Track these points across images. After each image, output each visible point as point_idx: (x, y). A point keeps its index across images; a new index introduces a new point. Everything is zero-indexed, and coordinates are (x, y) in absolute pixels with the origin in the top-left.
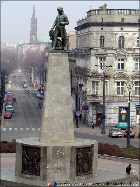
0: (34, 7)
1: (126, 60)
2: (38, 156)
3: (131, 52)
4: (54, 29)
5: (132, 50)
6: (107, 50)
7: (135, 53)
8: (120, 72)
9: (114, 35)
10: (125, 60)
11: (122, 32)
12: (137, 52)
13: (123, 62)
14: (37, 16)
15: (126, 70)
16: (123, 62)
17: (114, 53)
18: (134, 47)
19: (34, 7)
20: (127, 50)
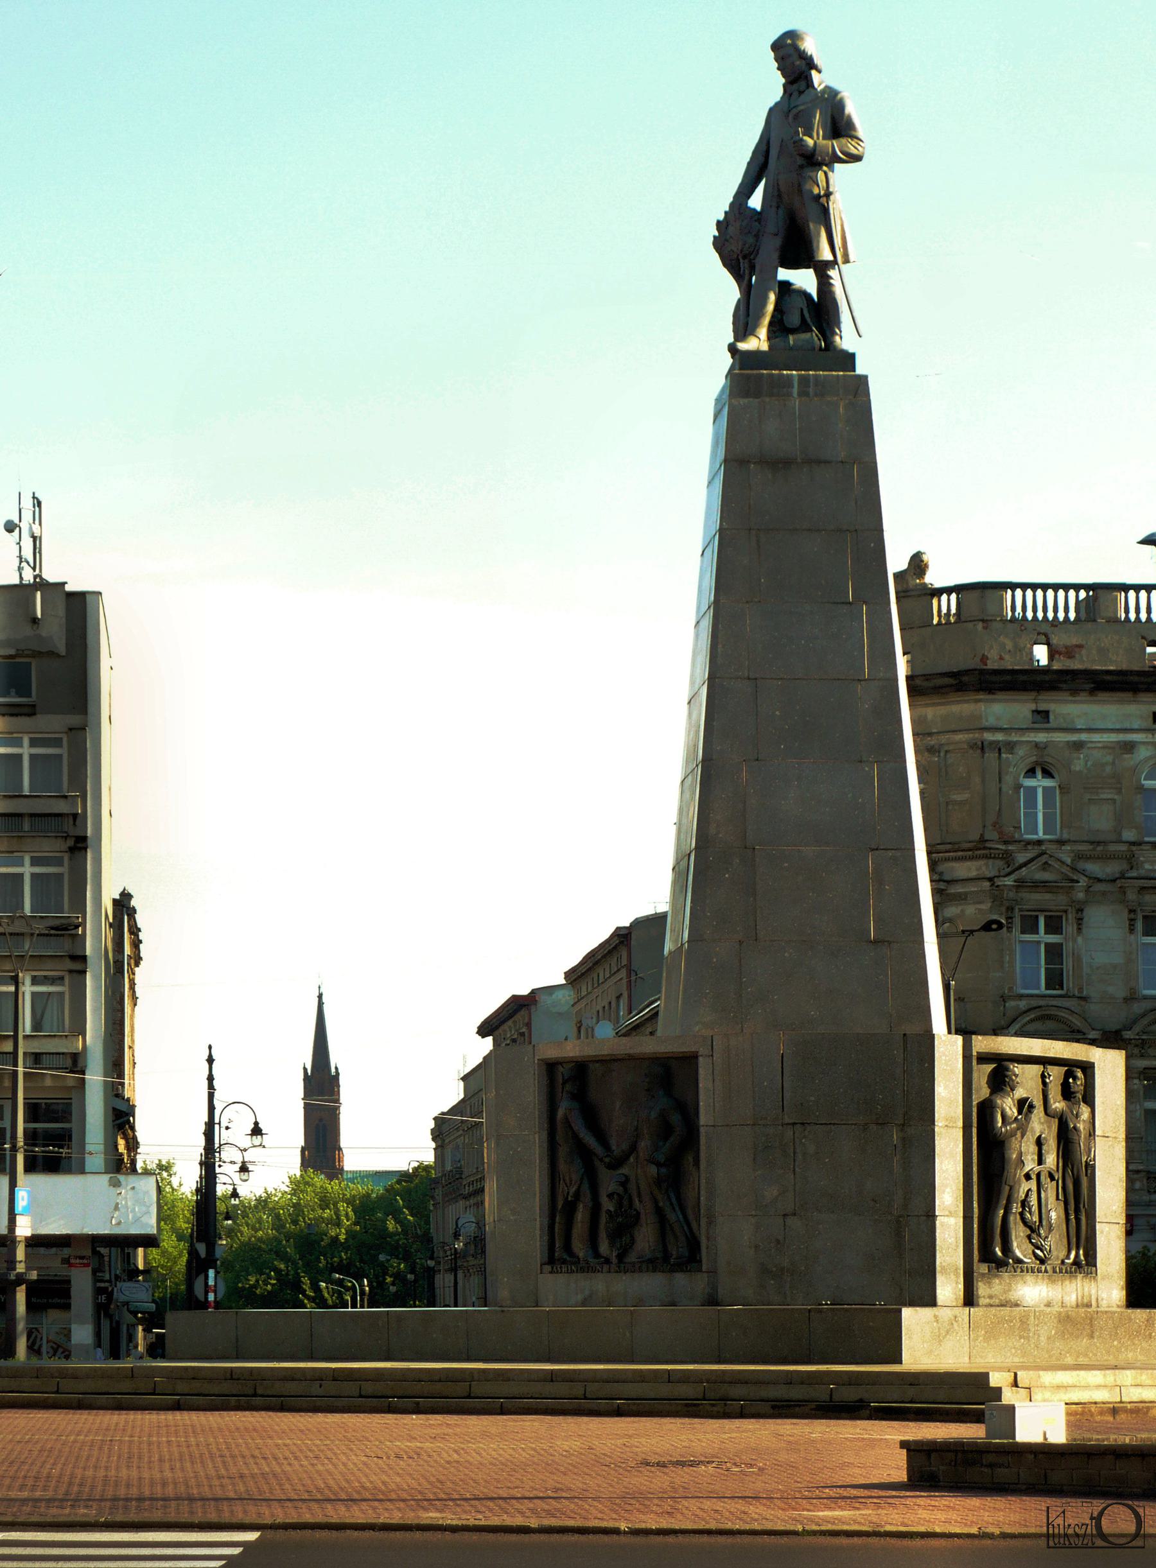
0: (320, 996)
1: (1079, 921)
2: (675, 1119)
3: (1112, 869)
4: (756, 201)
5: (1113, 857)
6: (947, 860)
7: (1134, 874)
8: (1042, 1002)
9: (991, 756)
10: (1069, 927)
11: (1041, 737)
12: (1147, 866)
13: (1053, 939)
14: (337, 1057)
15: (1081, 989)
16: (1053, 939)
17: (990, 879)
18: (1129, 835)
19: (320, 996)
20: (1080, 856)
